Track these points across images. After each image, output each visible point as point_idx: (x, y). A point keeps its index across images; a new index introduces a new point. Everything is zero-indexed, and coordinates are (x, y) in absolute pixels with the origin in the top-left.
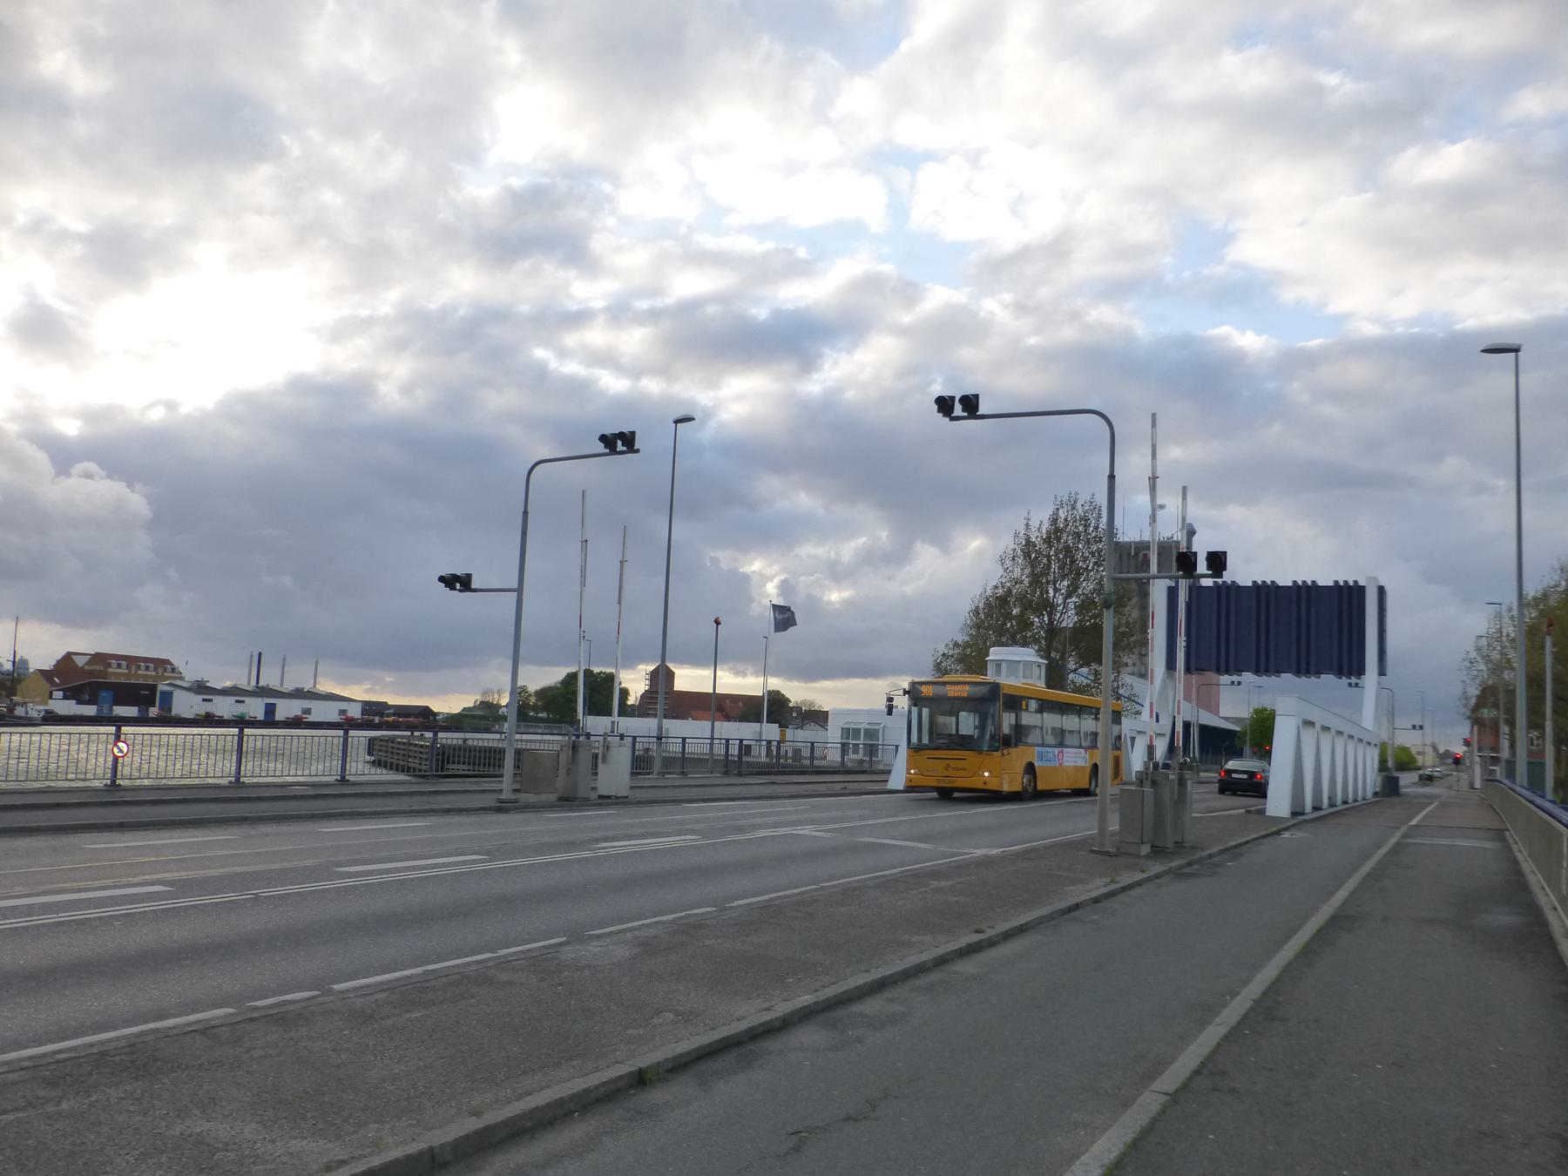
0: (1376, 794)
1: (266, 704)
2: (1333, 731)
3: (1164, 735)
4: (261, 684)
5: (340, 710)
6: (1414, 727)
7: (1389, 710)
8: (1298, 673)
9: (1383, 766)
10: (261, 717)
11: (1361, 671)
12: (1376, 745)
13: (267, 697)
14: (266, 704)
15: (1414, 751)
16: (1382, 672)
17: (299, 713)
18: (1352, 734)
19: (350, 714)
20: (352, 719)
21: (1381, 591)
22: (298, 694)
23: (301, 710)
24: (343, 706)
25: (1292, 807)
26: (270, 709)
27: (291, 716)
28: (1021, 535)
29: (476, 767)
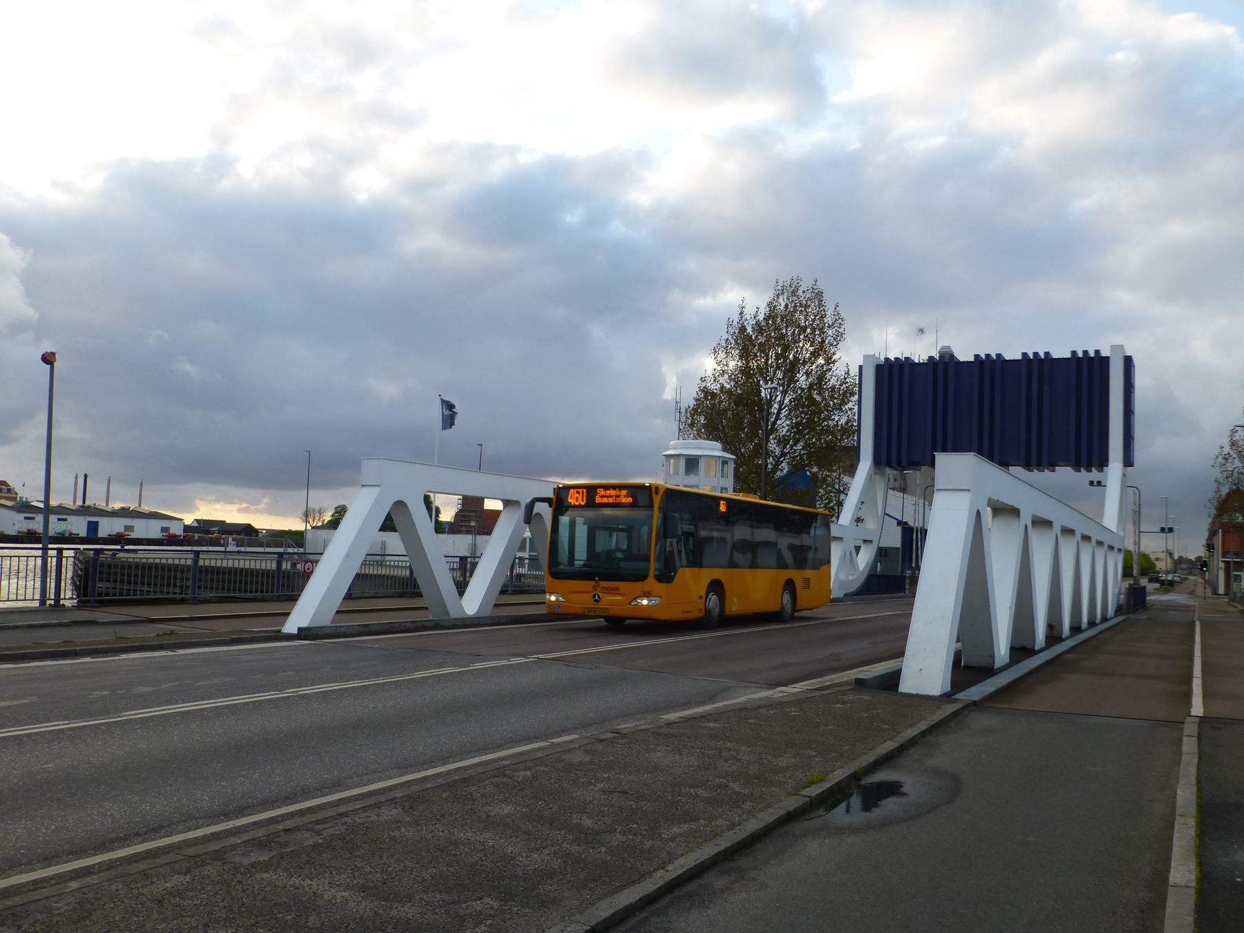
0: (1119, 610)
1: (89, 522)
2: (1078, 536)
3: (871, 541)
4: (87, 504)
5: (162, 528)
6: (1163, 530)
7: (1134, 512)
8: (1028, 466)
9: (1127, 573)
10: (83, 533)
11: (1101, 461)
12: (1120, 550)
13: (89, 515)
14: (89, 522)
15: (1153, 557)
16: (1128, 462)
17: (121, 530)
18: (1112, 544)
19: (172, 531)
20: (174, 536)
21: (1128, 362)
22: (124, 513)
23: (123, 528)
24: (165, 523)
25: (1011, 643)
26: (93, 527)
27: (114, 532)
28: (735, 323)
29: (118, 585)
